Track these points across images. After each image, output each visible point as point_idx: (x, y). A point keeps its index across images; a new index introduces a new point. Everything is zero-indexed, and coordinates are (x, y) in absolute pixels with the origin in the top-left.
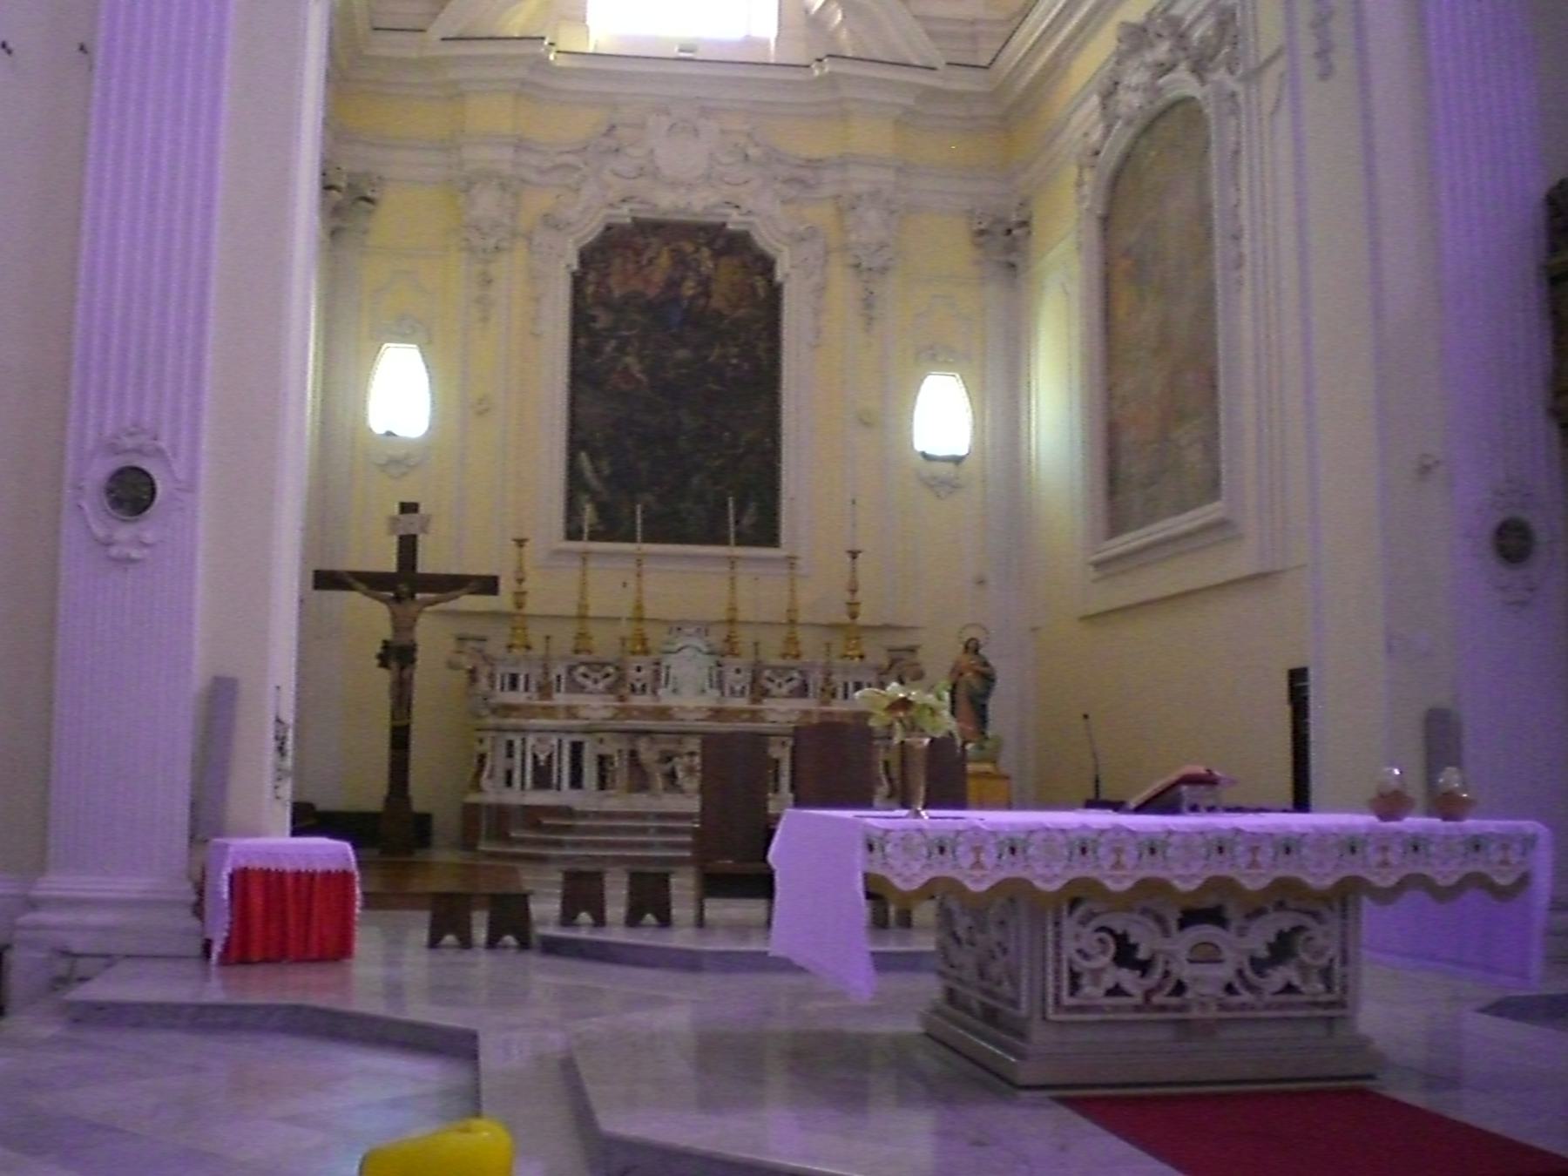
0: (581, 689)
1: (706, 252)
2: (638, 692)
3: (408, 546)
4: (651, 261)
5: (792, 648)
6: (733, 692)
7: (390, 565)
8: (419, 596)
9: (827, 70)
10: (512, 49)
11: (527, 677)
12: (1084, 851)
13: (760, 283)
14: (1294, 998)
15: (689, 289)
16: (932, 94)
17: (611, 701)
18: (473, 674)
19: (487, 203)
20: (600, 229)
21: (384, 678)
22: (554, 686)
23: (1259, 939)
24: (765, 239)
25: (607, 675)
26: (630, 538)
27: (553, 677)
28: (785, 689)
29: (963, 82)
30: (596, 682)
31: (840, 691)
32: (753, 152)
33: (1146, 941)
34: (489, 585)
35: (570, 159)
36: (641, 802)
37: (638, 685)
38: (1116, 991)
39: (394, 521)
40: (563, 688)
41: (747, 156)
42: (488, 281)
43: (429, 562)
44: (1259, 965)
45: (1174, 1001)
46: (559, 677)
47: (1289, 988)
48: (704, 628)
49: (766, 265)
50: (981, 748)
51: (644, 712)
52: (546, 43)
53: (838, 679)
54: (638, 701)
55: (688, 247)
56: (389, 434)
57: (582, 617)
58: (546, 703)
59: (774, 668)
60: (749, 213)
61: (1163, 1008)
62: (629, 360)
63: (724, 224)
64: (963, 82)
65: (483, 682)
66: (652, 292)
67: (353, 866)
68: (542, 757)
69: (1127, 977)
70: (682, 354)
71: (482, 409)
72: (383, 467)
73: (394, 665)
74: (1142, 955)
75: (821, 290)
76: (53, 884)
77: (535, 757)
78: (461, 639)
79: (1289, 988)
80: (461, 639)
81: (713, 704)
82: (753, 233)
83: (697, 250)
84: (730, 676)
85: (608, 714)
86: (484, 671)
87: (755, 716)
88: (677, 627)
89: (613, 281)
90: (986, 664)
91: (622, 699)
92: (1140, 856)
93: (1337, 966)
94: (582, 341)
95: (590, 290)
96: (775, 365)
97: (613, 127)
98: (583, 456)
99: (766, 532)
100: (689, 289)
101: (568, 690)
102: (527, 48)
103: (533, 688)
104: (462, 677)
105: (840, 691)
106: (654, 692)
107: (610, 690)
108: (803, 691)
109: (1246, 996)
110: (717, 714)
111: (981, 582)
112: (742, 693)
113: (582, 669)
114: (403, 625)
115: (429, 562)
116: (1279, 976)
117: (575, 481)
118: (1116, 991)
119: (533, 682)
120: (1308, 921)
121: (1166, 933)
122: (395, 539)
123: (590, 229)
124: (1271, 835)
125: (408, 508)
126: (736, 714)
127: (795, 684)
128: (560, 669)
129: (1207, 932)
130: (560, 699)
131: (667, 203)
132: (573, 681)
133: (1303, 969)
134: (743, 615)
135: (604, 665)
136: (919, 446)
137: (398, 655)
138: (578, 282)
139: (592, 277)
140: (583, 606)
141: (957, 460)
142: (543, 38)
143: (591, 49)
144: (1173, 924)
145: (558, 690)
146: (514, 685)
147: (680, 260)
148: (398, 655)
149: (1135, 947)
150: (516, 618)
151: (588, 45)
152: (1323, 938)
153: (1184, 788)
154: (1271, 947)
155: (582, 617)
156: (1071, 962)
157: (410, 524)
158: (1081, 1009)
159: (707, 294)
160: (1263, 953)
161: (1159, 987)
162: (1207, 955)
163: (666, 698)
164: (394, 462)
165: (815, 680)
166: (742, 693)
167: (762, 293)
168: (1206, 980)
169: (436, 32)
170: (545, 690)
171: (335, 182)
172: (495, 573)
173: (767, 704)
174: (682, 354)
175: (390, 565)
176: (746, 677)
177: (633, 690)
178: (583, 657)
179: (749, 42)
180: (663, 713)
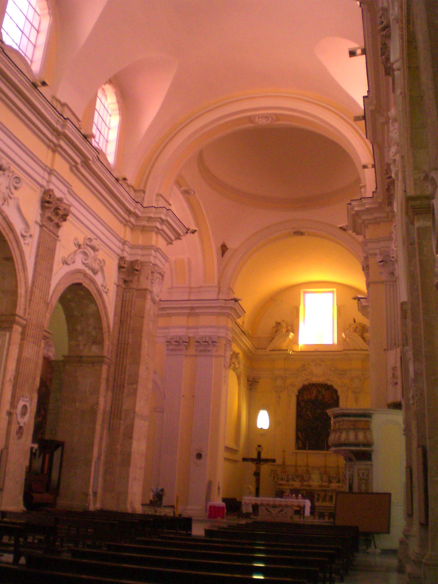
0: (295, 481)
1: (323, 390)
3: (259, 454)
7: (255, 456)
10: (283, 352)
13: (335, 395)
15: (320, 397)
18: (274, 477)
19: (279, 382)
21: (254, 478)
23: (280, 509)
32: (332, 369)
34: (274, 461)
36: (324, 504)
42: (279, 398)
43: (263, 456)
44: (279, 512)
49: (336, 392)
51: (307, 486)
55: (320, 389)
56: (261, 428)
60: (332, 381)
62: (309, 413)
65: (276, 479)
66: (313, 398)
67: (225, 506)
70: (318, 411)
76: (190, 507)
78: (272, 471)
98: (299, 433)
102: (285, 352)
108: (339, 482)
110: (321, 486)
114: (258, 468)
115: (263, 456)
117: (298, 438)
125: (259, 446)
127: (337, 480)
128: (291, 477)
130: (291, 483)
131: (315, 380)
137: (257, 474)
138: (298, 397)
142: (288, 350)
146: (282, 480)
148: (257, 474)
150: (284, 465)
157: (260, 449)
160: (280, 511)
163: (311, 483)
167: (335, 398)
169: (268, 350)
170: (288, 481)
171: (250, 380)
174: (318, 411)
175: (255, 456)
179: (333, 345)
180: (310, 486)
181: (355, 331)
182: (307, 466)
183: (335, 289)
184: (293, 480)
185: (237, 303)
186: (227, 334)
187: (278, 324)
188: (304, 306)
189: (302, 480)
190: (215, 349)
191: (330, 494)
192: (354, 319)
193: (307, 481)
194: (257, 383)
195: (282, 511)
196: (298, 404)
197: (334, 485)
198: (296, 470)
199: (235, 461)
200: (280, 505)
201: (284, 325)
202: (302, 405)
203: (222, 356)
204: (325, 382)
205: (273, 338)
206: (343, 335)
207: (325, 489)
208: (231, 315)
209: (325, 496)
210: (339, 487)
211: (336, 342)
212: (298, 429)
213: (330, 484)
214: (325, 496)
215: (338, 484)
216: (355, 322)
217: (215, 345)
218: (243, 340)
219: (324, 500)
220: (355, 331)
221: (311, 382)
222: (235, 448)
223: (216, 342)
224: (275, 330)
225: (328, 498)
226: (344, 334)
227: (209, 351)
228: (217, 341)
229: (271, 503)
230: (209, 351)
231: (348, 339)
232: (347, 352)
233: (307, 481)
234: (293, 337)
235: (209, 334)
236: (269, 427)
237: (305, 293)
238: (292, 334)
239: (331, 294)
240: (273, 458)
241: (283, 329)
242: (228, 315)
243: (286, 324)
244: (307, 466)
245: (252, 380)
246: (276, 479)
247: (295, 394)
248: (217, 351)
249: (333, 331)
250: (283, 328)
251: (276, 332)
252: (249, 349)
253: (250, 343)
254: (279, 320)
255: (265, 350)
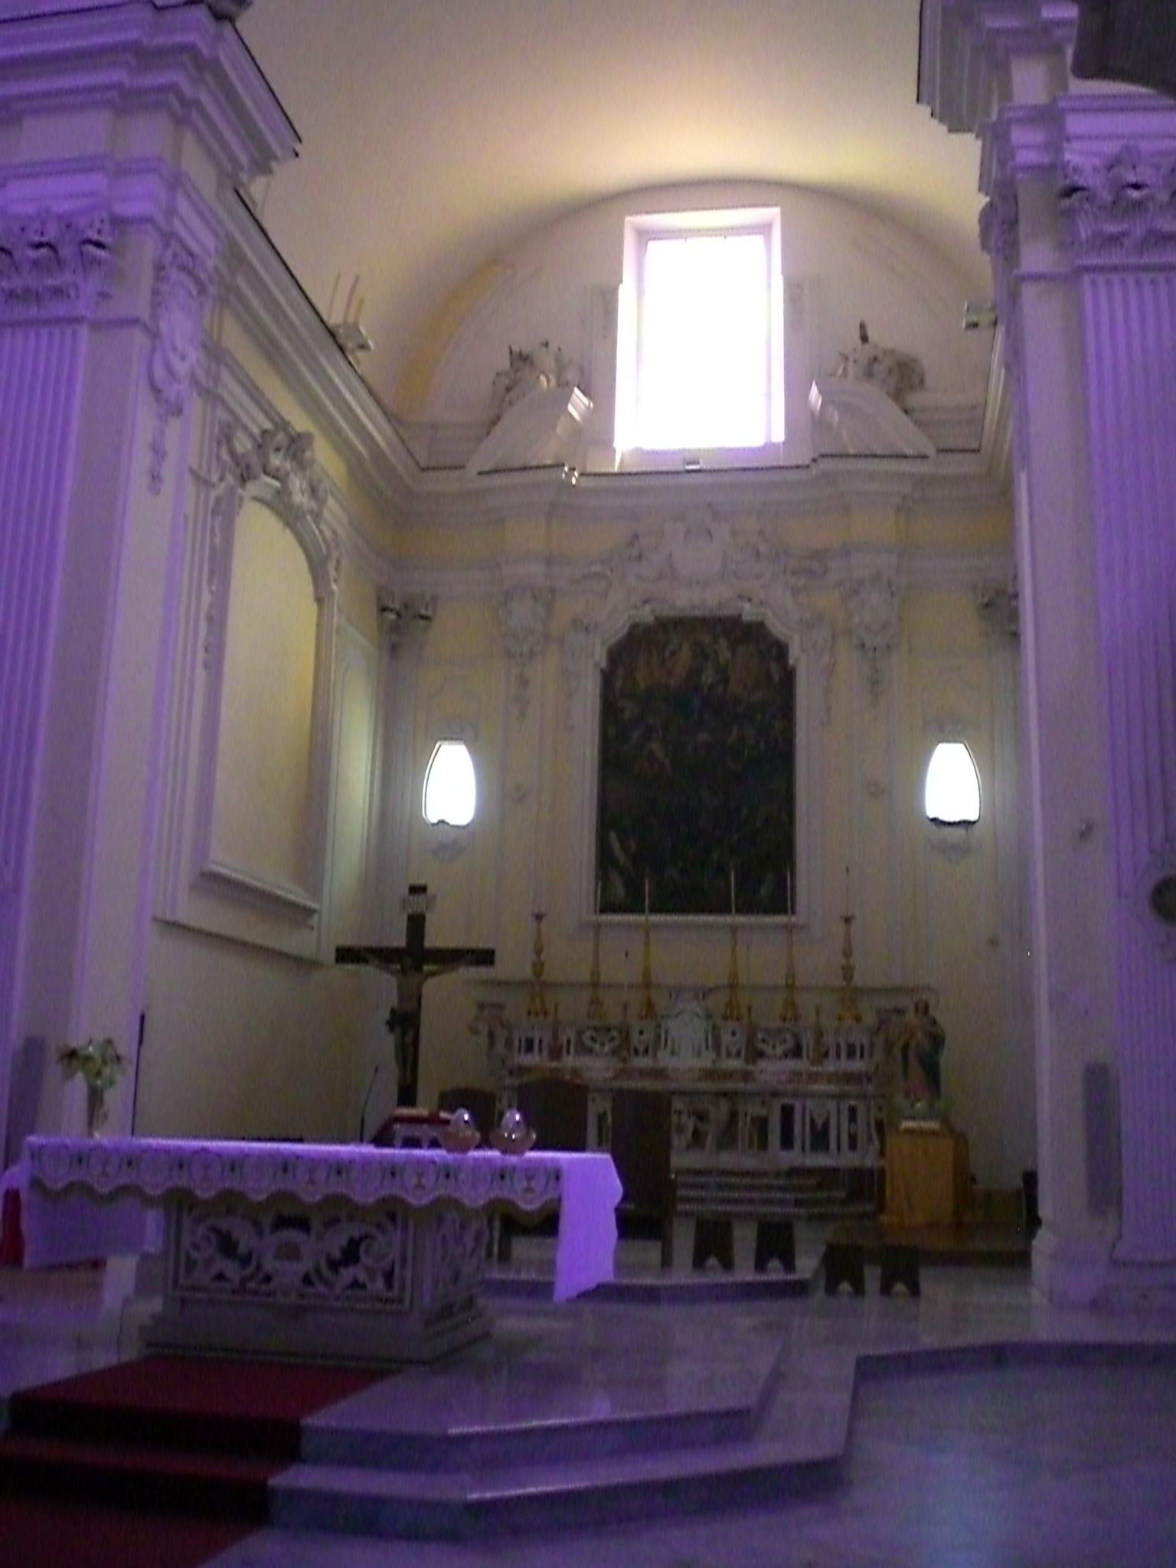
0: (590, 1051)
1: (723, 643)
2: (641, 1055)
3: (416, 924)
4: (673, 653)
5: (792, 1007)
6: (729, 1055)
7: (398, 939)
8: (426, 968)
9: (814, 472)
10: (542, 476)
11: (541, 1042)
12: (233, 1168)
13: (774, 668)
14: (360, 1293)
15: (708, 677)
16: (924, 482)
17: (614, 1063)
18: (491, 1036)
19: (522, 613)
20: (625, 630)
22: (564, 1049)
23: (335, 1243)
24: (777, 628)
25: (612, 1039)
26: (724, 909)
27: (565, 1039)
28: (779, 1051)
29: (952, 466)
30: (603, 1044)
31: (832, 1052)
32: (762, 548)
33: (245, 1239)
34: (485, 957)
35: (596, 568)
36: (727, 1160)
37: (641, 1049)
38: (220, 1276)
39: (404, 903)
40: (572, 1050)
41: (758, 553)
42: (524, 682)
43: (436, 937)
44: (334, 1266)
45: (264, 1287)
46: (569, 1042)
47: (355, 1284)
48: (705, 993)
49: (781, 650)
50: (931, 1106)
51: (643, 1073)
52: (566, 469)
53: (829, 1040)
54: (644, 1062)
55: (707, 639)
56: (442, 822)
57: (595, 984)
58: (554, 1064)
59: (767, 1031)
61: (256, 1293)
62: (656, 747)
63: (740, 616)
64: (952, 466)
65: (500, 1047)
68: (820, 1122)
69: (232, 1269)
70: (703, 737)
71: (520, 797)
72: (435, 853)
73: (398, 1030)
74: (242, 1249)
75: (830, 671)
77: (812, 1120)
78: (481, 1006)
79: (355, 1284)
80: (481, 1006)
81: (709, 1065)
82: (766, 622)
83: (715, 641)
84: (726, 1038)
85: (608, 1075)
86: (501, 1036)
87: (747, 1076)
88: (677, 992)
89: (639, 676)
90: (934, 1022)
91: (624, 1060)
92: (275, 1174)
93: (397, 1270)
94: (612, 731)
95: (618, 684)
96: (790, 742)
97: (636, 536)
98: (613, 836)
99: (781, 901)
100: (708, 677)
101: (577, 1052)
102: (553, 474)
103: (545, 1052)
104: (483, 1040)
105: (832, 1052)
106: (655, 1055)
107: (614, 1052)
108: (796, 1052)
109: (321, 1288)
110: (709, 1074)
111: (993, 942)
112: (738, 1054)
113: (589, 1033)
115: (436, 937)
116: (347, 1274)
118: (220, 1276)
119: (545, 1044)
120: (375, 1231)
121: (260, 1233)
122: (405, 917)
123: (617, 627)
124: (326, 1161)
125: (417, 890)
126: (728, 1075)
129: (293, 1235)
130: (570, 1061)
131: (686, 600)
132: (583, 1044)
133: (370, 1271)
134: (743, 980)
135: (609, 1029)
136: (931, 813)
138: (607, 678)
139: (621, 671)
140: (595, 972)
141: (966, 824)
142: (563, 465)
143: (616, 469)
144: (267, 1229)
145: (568, 1052)
147: (701, 653)
149: (236, 1244)
150: (538, 984)
151: (613, 467)
152: (387, 1246)
153: (397, 1126)
154: (344, 1251)
155: (595, 984)
156: (188, 1254)
157: (418, 903)
158: (194, 1288)
159: (726, 681)
160: (337, 1254)
161: (252, 1277)
162: (291, 1253)
163: (664, 1059)
164: (443, 847)
165: (808, 1040)
166: (738, 1054)
167: (776, 678)
168: (288, 1273)
169: (473, 469)
170: (556, 1053)
171: (391, 605)
172: (489, 945)
173: (763, 1064)
175: (398, 939)
176: (741, 1039)
177: (636, 1052)
178: (596, 1022)
179: (769, 447)
180: (659, 1073)
181: (869, 375)
182: (647, 984)
183: (773, 213)
184: (585, 1050)
185: (227, 29)
186: (171, 212)
187: (521, 360)
188: (640, 291)
189: (624, 1047)
190: (91, 285)
191: (755, 1110)
192: (862, 327)
193: (646, 1051)
194: (422, 623)
195: (351, 1254)
196: (609, 710)
197: (772, 1070)
198: (595, 1002)
199: (303, 964)
200: (337, 1209)
201: (547, 360)
202: (627, 715)
203: (134, 322)
204: (729, 611)
205: (498, 418)
206: (814, 395)
207: (729, 1086)
208: (197, 104)
209: (733, 1116)
210: (796, 1075)
211: (779, 436)
212: (606, 821)
213: (754, 1062)
214: (733, 1116)
215: (791, 1064)
216: (864, 339)
217: (98, 262)
218: (337, 380)
219: (728, 1139)
220: (869, 375)
221: (668, 612)
222: (297, 895)
223: (99, 245)
224: (507, 381)
225: (743, 1126)
226: (820, 391)
227: (58, 292)
228: (104, 239)
229: (259, 1190)
230: (58, 292)
231: (835, 416)
232: (826, 465)
233: (646, 1051)
234: (590, 416)
235: (67, 206)
236: (473, 821)
237: (645, 236)
238: (578, 404)
239: (758, 240)
240: (478, 941)
241: (542, 378)
242: (184, 114)
243: (557, 360)
244: (647, 984)
245: (397, 606)
246: (500, 1047)
247: (597, 664)
248: (104, 295)
249: (769, 395)
250: (543, 372)
251: (508, 389)
252: (378, 455)
253: (389, 431)
254: (523, 343)
255: (457, 473)
